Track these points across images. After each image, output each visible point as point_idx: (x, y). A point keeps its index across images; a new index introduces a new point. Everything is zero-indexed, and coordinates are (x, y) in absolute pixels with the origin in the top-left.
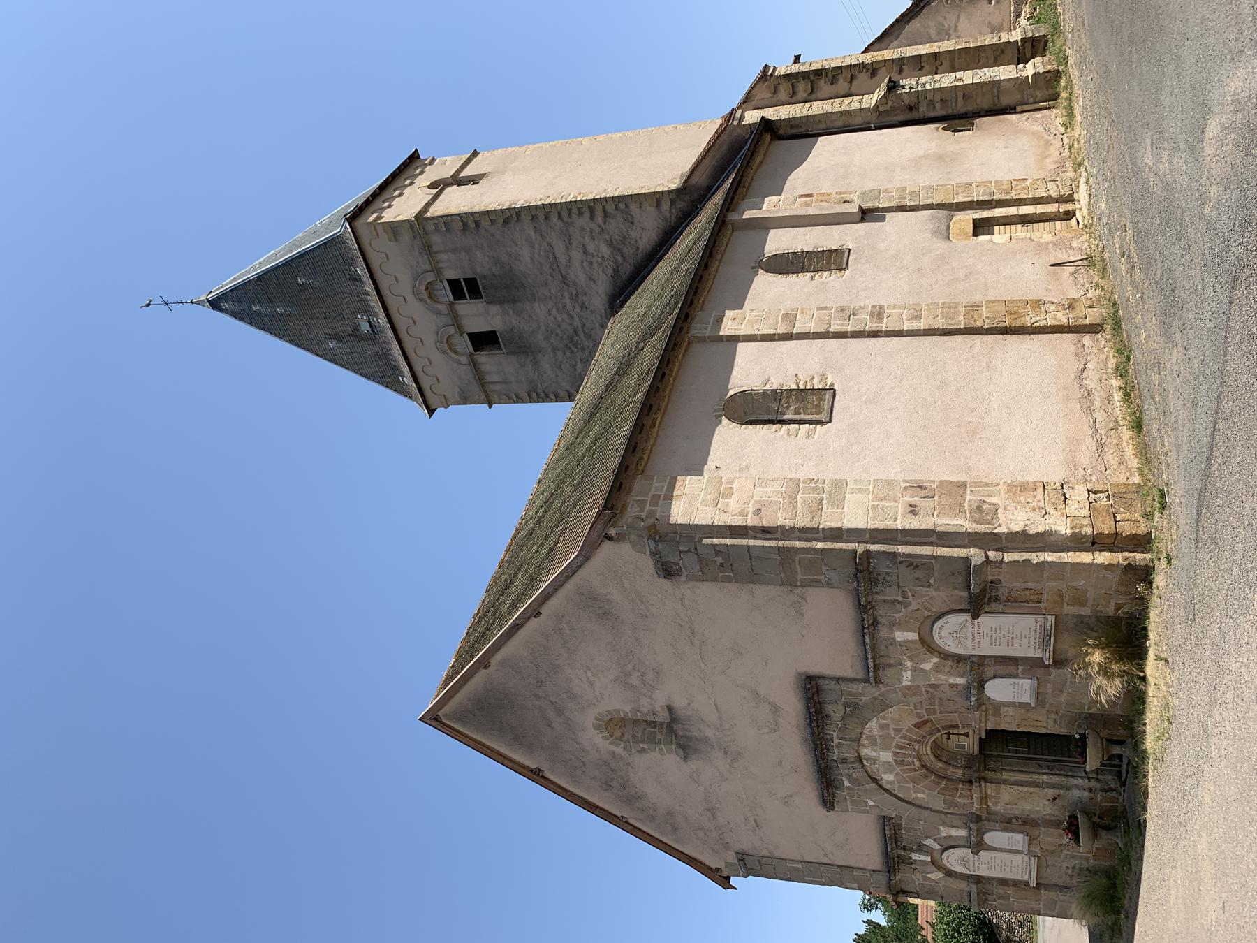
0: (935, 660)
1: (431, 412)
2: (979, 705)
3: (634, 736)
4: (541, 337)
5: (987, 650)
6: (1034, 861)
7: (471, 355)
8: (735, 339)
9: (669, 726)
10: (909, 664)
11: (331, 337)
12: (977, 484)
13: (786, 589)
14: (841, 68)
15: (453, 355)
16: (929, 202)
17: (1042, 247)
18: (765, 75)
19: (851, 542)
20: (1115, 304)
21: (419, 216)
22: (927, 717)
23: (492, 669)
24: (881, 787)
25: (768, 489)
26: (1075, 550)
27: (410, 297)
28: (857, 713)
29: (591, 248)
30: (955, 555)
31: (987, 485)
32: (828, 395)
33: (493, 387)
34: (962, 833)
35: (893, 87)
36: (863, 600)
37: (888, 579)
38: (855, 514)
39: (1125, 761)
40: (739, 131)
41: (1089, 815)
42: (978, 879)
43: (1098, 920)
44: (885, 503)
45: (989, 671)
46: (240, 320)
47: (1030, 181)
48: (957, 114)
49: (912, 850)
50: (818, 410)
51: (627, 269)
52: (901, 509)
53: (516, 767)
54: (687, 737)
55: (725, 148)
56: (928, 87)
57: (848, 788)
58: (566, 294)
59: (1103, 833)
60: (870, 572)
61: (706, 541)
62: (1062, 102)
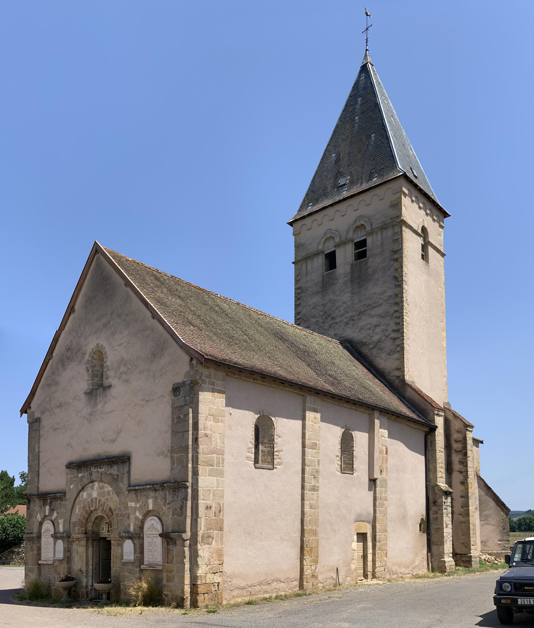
0: (140, 517)
1: (291, 224)
2: (121, 537)
3: (95, 366)
4: (331, 297)
5: (146, 541)
6: (51, 562)
7: (323, 252)
8: (303, 419)
9: (101, 385)
10: (138, 505)
11: (338, 155)
12: (222, 536)
13: (170, 448)
14: (467, 466)
15: (323, 240)
16: (378, 512)
17: (348, 564)
18: (467, 426)
19: (192, 480)
20: (310, 594)
21: (404, 223)
22: (114, 513)
23: (125, 288)
24: (80, 492)
25: (218, 440)
26: (191, 577)
27: (357, 214)
28: (115, 480)
29: (378, 330)
30: (187, 526)
31: (222, 540)
32: (270, 466)
33: (304, 265)
34: (61, 529)
35: (447, 494)
36: (165, 485)
37: (176, 496)
38: (205, 481)
39: (100, 601)
40: (431, 414)
41: (75, 585)
42: (39, 537)
43: (26, 590)
44: (211, 495)
45: (136, 541)
46: (353, 88)
47: (385, 559)
48: (429, 526)
49: (50, 506)
50: (264, 461)
51: (365, 350)
52: (209, 502)
53: (74, 298)
54: (97, 394)
55: (423, 406)
56: (444, 511)
57: (78, 476)
58: (354, 313)
59: (67, 592)
60: (178, 488)
61: (191, 410)
62: (432, 575)
